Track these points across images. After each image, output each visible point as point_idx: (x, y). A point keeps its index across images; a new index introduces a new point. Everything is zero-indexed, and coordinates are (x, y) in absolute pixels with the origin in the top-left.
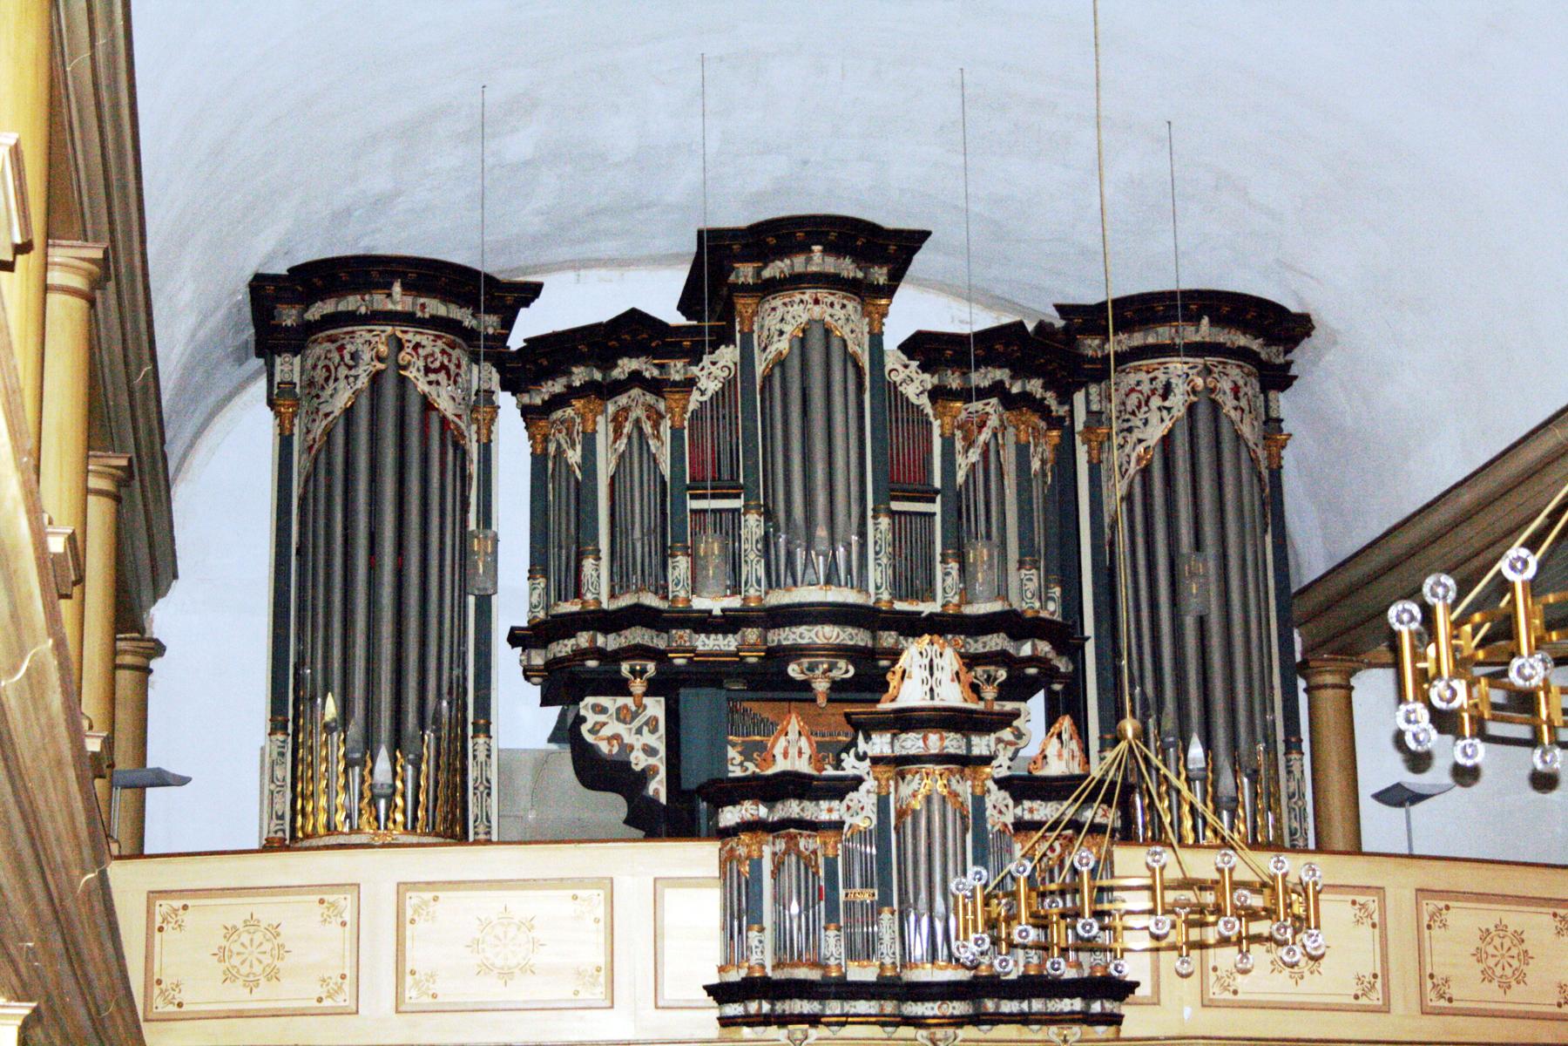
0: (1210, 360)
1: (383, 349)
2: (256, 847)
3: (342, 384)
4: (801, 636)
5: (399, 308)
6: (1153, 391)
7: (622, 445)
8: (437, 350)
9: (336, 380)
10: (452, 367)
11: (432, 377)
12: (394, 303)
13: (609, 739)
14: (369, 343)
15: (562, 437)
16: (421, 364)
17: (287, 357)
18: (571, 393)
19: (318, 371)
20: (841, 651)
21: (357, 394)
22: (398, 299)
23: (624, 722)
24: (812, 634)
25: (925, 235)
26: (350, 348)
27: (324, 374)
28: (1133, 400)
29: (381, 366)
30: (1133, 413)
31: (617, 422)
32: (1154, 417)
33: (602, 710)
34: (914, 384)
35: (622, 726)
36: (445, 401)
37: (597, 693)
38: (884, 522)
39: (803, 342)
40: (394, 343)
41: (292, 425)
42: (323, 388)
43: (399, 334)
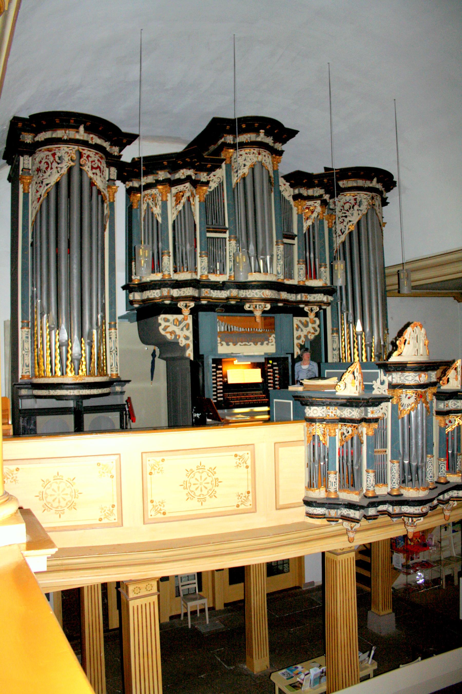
0: (374, 194)
1: (75, 157)
2: (45, 569)
3: (55, 170)
4: (256, 294)
5: (81, 138)
6: (356, 203)
7: (180, 207)
8: (96, 160)
9: (52, 168)
10: (102, 168)
11: (94, 171)
12: (80, 136)
13: (171, 333)
14: (66, 152)
15: (150, 202)
16: (89, 164)
17: (26, 157)
18: (158, 182)
19: (43, 163)
20: (266, 300)
21: (62, 175)
22: (81, 134)
23: (176, 325)
24: (261, 294)
25: (296, 132)
26: (58, 154)
27: (46, 166)
28: (347, 206)
29: (72, 164)
30: (348, 211)
31: (178, 197)
32: (356, 213)
33: (167, 320)
34: (287, 191)
35: (175, 327)
36: (100, 183)
37: (165, 313)
38: (281, 247)
39: (253, 169)
40: (78, 155)
41: (29, 188)
42: (45, 172)
43: (81, 151)
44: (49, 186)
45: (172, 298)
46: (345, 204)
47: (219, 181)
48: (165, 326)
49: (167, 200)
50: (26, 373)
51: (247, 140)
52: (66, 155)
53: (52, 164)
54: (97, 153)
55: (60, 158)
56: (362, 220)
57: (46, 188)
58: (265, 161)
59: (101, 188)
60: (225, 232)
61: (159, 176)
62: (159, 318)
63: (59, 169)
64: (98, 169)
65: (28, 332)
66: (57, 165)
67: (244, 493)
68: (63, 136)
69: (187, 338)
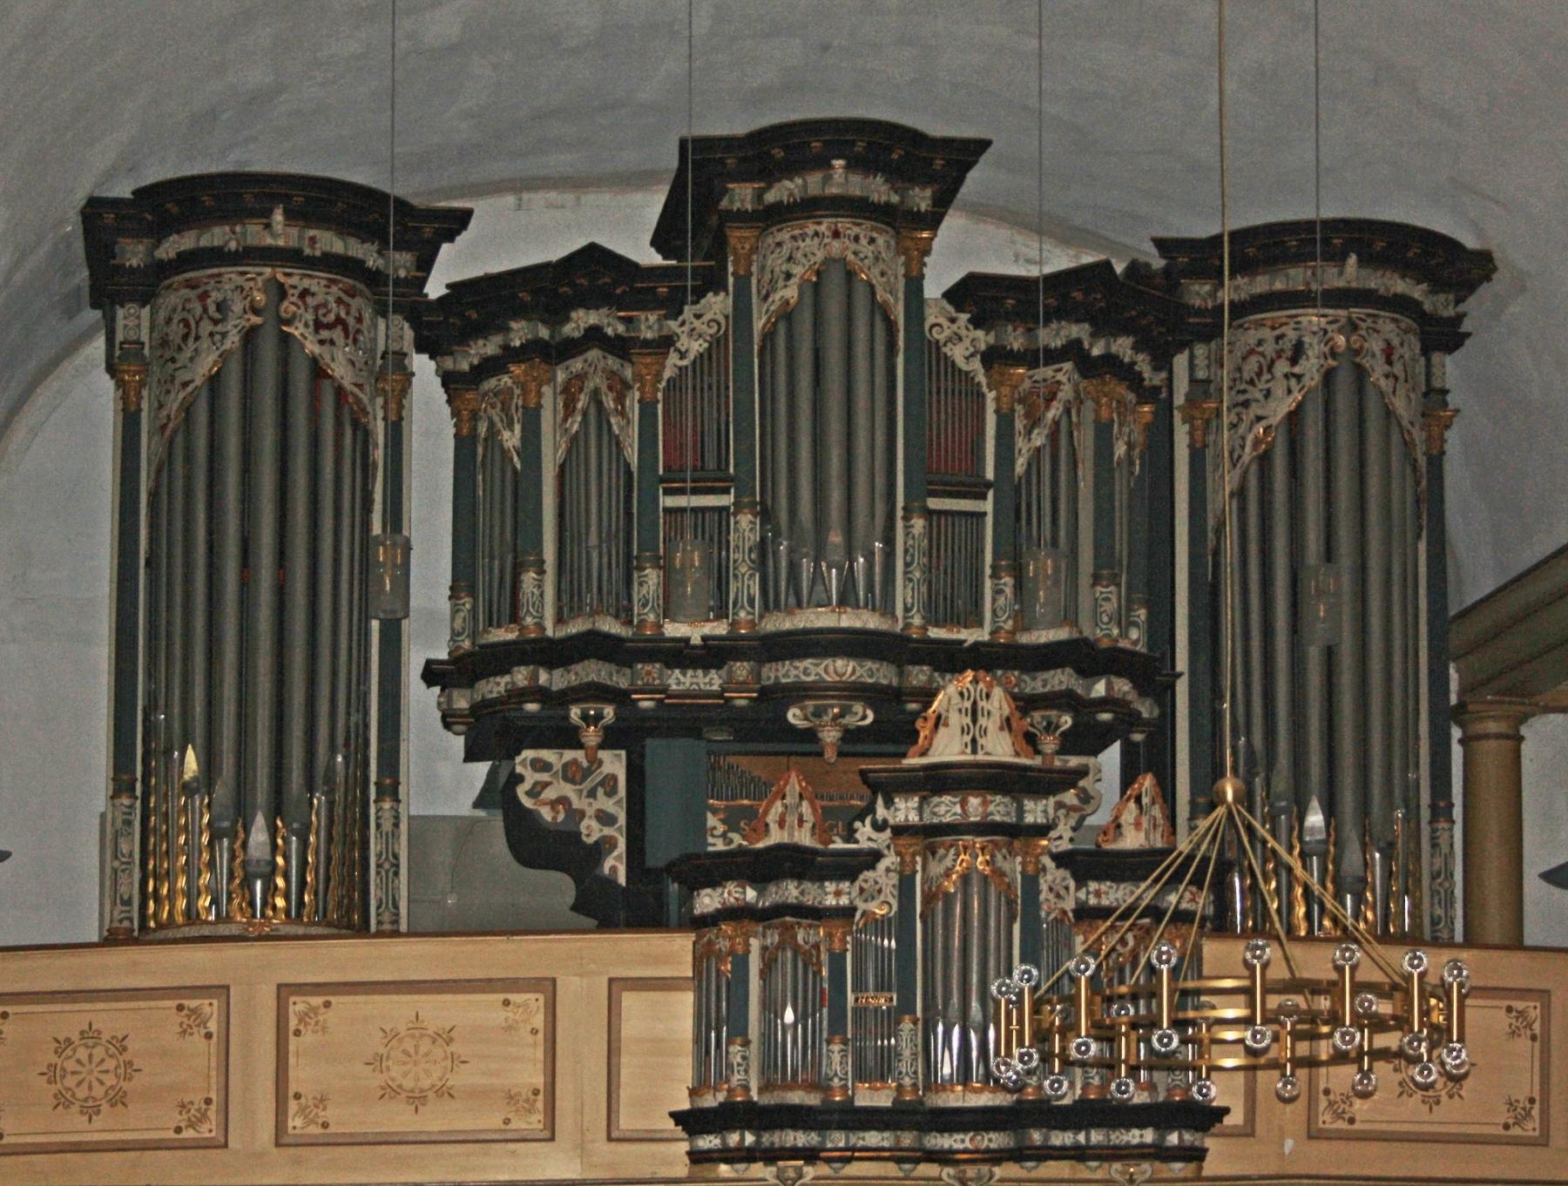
0: (1356, 312)
3: (205, 343)
4: (806, 672)
8: (331, 299)
9: (197, 338)
10: (351, 321)
11: (325, 334)
13: (553, 804)
14: (241, 288)
15: (495, 414)
17: (132, 308)
18: (510, 355)
19: (174, 326)
20: (857, 691)
24: (820, 670)
26: (216, 295)
27: (182, 330)
31: (569, 394)
34: (964, 345)
38: (919, 524)
39: (816, 288)
41: (140, 397)
42: (180, 349)
44: (190, 389)
45: (542, 694)
46: (1244, 359)
47: (713, 331)
48: (536, 784)
49: (539, 406)
50: (121, 921)
51: (791, 194)
52: (237, 296)
53: (197, 323)
54: (333, 281)
55: (220, 306)
56: (1309, 407)
57: (181, 395)
58: (856, 253)
59: (347, 384)
60: (726, 491)
61: (512, 335)
62: (518, 759)
63: (217, 337)
64: (339, 328)
65: (130, 807)
66: (210, 328)
67: (524, 1092)
68: (227, 243)
69: (605, 818)
